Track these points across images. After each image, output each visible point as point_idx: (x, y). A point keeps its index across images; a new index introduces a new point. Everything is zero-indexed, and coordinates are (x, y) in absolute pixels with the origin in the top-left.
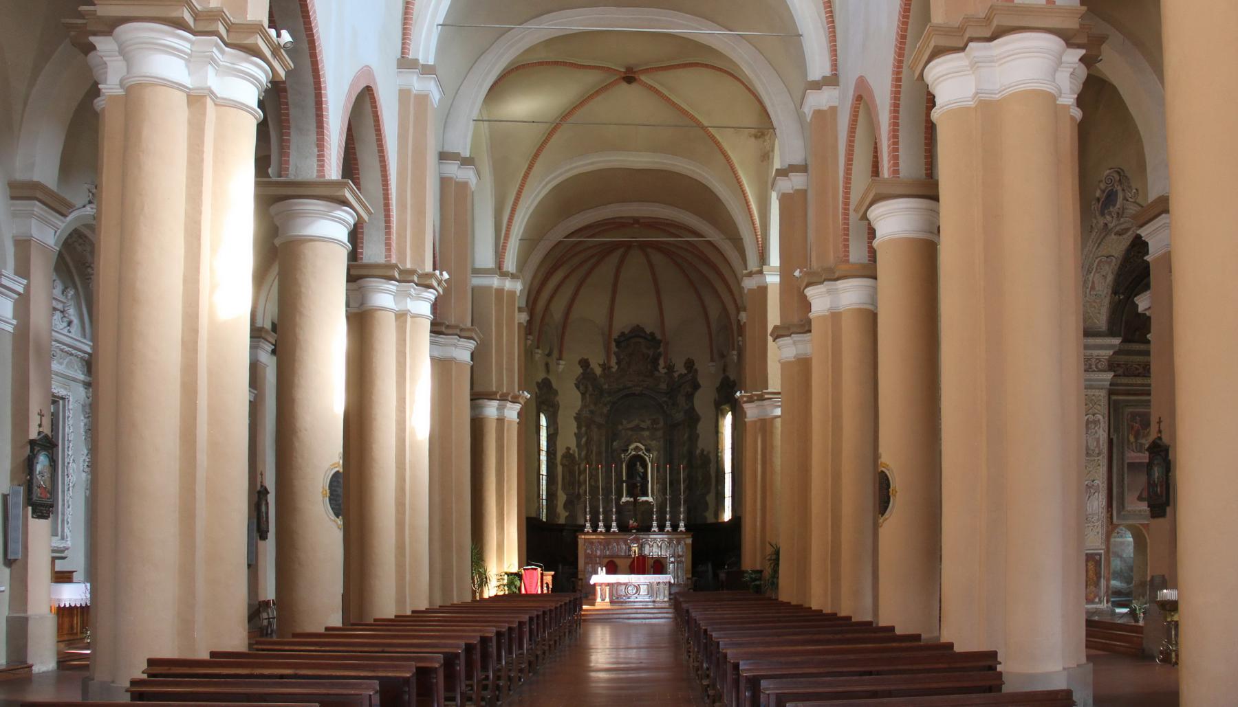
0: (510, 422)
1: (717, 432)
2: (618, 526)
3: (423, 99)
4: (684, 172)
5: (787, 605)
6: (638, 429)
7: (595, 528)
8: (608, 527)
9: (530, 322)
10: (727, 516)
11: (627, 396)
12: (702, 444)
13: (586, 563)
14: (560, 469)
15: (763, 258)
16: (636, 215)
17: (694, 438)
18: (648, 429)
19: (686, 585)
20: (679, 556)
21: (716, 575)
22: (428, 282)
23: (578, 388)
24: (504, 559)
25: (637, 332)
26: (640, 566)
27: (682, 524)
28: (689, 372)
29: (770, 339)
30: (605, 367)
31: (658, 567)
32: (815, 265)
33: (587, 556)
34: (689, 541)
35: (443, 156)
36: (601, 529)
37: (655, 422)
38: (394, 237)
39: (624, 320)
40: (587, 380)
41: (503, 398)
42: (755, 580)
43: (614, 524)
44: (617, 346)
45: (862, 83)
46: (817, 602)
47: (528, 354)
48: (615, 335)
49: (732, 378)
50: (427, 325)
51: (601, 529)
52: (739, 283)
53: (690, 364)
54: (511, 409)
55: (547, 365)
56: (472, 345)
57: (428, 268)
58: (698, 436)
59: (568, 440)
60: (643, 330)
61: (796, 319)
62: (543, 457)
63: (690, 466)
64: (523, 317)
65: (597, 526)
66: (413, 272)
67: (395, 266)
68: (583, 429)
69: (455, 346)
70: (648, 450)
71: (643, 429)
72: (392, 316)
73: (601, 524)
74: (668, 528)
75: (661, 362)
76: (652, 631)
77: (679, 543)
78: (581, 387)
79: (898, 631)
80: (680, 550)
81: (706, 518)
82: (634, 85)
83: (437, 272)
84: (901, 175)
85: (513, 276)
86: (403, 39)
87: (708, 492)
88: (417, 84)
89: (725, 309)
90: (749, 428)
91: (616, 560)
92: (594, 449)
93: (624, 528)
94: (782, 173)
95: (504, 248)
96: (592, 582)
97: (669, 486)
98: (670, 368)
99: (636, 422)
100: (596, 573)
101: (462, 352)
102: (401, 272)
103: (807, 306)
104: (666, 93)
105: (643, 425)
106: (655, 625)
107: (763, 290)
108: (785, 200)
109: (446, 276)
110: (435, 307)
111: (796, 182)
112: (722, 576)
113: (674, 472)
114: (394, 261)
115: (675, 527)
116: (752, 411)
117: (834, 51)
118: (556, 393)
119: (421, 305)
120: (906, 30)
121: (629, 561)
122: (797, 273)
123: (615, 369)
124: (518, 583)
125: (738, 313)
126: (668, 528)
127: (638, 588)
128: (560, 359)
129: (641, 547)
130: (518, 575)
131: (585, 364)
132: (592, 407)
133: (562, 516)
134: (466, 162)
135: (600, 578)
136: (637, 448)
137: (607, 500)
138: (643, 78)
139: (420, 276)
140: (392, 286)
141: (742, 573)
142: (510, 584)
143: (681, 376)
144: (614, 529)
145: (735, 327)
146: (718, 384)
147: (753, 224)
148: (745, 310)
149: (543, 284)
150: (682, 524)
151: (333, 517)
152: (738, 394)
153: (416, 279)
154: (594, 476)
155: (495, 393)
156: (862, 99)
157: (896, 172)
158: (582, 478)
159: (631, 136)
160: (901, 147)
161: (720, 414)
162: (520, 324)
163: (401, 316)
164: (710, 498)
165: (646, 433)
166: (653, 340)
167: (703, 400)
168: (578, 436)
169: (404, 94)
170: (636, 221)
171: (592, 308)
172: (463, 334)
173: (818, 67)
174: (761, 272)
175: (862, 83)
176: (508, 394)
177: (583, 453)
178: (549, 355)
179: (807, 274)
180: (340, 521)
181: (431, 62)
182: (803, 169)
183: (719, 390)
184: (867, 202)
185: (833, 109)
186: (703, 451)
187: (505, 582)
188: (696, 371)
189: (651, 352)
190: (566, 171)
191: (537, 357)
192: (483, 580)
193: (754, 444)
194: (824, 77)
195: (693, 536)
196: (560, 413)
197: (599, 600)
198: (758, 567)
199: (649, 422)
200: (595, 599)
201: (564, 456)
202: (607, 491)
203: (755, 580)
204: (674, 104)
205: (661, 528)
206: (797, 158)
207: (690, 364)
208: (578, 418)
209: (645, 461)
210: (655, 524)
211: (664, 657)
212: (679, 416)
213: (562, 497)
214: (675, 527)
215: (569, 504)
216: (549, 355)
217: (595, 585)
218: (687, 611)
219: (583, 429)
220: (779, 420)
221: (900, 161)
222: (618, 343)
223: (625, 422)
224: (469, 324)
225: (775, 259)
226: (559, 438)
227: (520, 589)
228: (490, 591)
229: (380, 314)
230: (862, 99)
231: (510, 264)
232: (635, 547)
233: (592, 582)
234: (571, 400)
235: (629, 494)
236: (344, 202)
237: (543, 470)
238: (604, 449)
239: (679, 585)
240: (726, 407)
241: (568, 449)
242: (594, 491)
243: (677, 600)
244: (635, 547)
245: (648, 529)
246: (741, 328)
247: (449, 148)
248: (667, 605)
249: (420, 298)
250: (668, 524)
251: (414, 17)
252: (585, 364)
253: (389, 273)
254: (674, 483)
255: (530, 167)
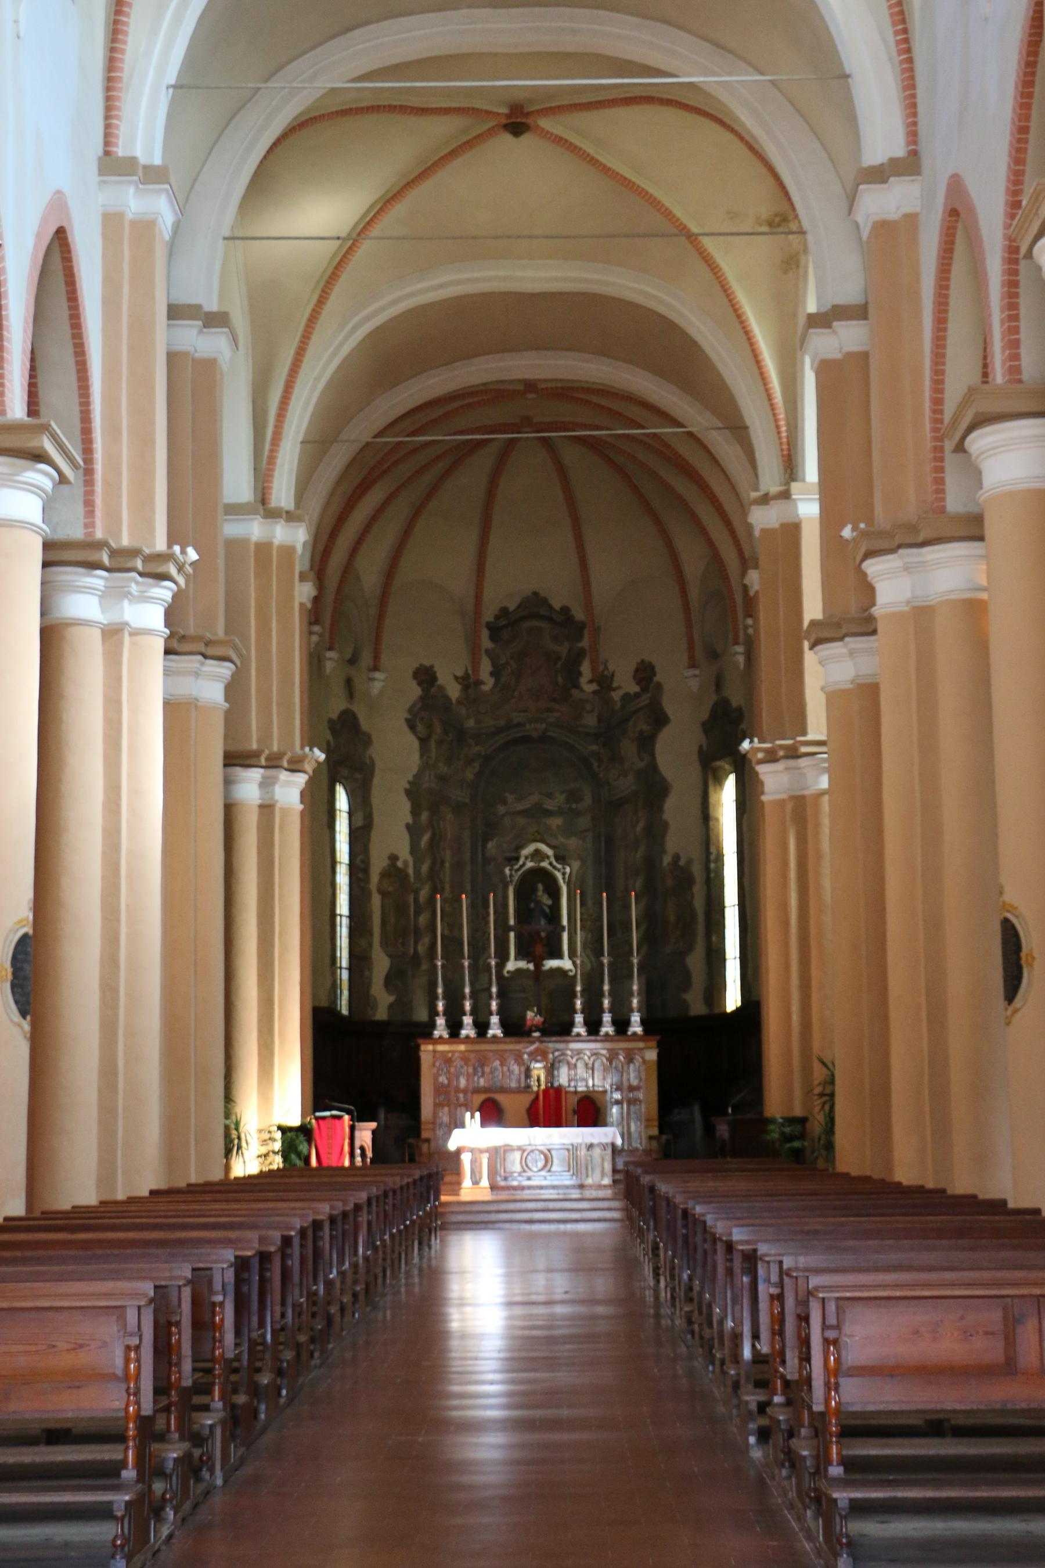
0: (285, 811)
1: (706, 817)
2: (503, 1024)
3: (145, 227)
4: (627, 295)
5: (846, 1176)
6: (538, 812)
7: (454, 1028)
8: (482, 1027)
9: (316, 600)
10: (733, 1000)
11: (517, 741)
12: (677, 843)
13: (437, 1106)
14: (376, 901)
15: (791, 468)
16: (528, 375)
17: (656, 832)
18: (560, 812)
19: (647, 1152)
20: (632, 1089)
21: (709, 1130)
22: (161, 569)
23: (412, 727)
24: (274, 1098)
25: (535, 606)
26: (549, 1109)
27: (636, 1018)
28: (644, 690)
29: (806, 644)
30: (469, 682)
31: (589, 1111)
32: (882, 517)
33: (440, 1090)
34: (652, 1055)
35: (175, 312)
36: (468, 1030)
37: (573, 796)
38: (99, 488)
39: (504, 588)
40: (430, 711)
41: (273, 763)
42: (789, 1138)
43: (495, 1020)
44: (493, 638)
45: (956, 186)
46: (905, 1174)
47: (314, 662)
48: (488, 616)
49: (735, 701)
50: (159, 645)
51: (468, 1030)
52: (744, 513)
53: (645, 673)
54: (288, 784)
55: (349, 682)
56: (225, 670)
57: (160, 544)
58: (665, 826)
59: (393, 840)
60: (545, 602)
61: (853, 608)
62: (342, 878)
63: (650, 891)
64: (304, 592)
65: (460, 1025)
66: (133, 553)
67: (99, 545)
68: (424, 816)
69: (197, 674)
70: (560, 858)
71: (549, 813)
72: (97, 634)
73: (467, 1020)
74: (607, 1028)
75: (586, 668)
76: (579, 1246)
77: (630, 1060)
78: (420, 728)
79: (1011, 1205)
80: (633, 1077)
81: (685, 1005)
82: (526, 138)
83: (177, 549)
84: (1025, 376)
85: (290, 517)
86: (107, 117)
87: (690, 948)
88: (135, 201)
89: (716, 557)
90: (768, 810)
91: (500, 1098)
92: (448, 856)
93: (514, 1029)
94: (822, 320)
95: (272, 460)
96: (452, 1145)
97: (604, 937)
98: (604, 682)
99: (535, 798)
100: (462, 1125)
101: (209, 684)
102: (114, 553)
103: (869, 591)
104: (591, 151)
105: (550, 805)
106: (586, 1234)
107: (792, 530)
108: (825, 370)
109: (192, 555)
110: (171, 616)
111: (847, 338)
112: (723, 1130)
113: (620, 906)
114: (99, 535)
115: (621, 1025)
116: (774, 781)
117: (911, 107)
118: (367, 740)
119: (148, 612)
120: (1028, 118)
121: (526, 1100)
122: (847, 532)
123: (488, 684)
124: (303, 1147)
125: (744, 574)
126: (607, 1028)
127: (548, 1159)
128: (376, 668)
129: (551, 1070)
130: (304, 1130)
131: (425, 676)
132: (444, 769)
133: (382, 1003)
134: (215, 320)
135: (471, 1137)
136: (537, 855)
137: (479, 969)
138: (544, 123)
139: (148, 559)
140: (98, 580)
141: (765, 1122)
142: (288, 1150)
143: (627, 698)
144: (495, 1030)
145: (739, 598)
146: (705, 716)
147: (770, 398)
148: (756, 567)
149: (341, 519)
150: (636, 1018)
151: (16, 1016)
152: (746, 745)
153: (139, 564)
154: (452, 919)
155: (256, 755)
156: (957, 215)
157: (1014, 371)
158: (423, 919)
159: (518, 235)
160: (1023, 324)
161: (711, 778)
162: (302, 605)
163: (113, 633)
164: (695, 961)
165: (556, 822)
166: (567, 624)
167: (675, 750)
168: (413, 831)
169: (112, 221)
170: (530, 386)
171: (443, 560)
172: (211, 651)
173: (882, 138)
174: (786, 495)
175: (956, 186)
176: (279, 756)
177: (425, 868)
178: (352, 661)
179: (863, 534)
180: (26, 1025)
181: (157, 161)
182: (859, 312)
183: (707, 727)
184: (964, 425)
185: (911, 221)
186: (676, 858)
187: (277, 1146)
188: (659, 686)
189: (563, 650)
190: (394, 302)
191: (329, 666)
192: (231, 1145)
193: (779, 847)
194: (893, 161)
195: (660, 1045)
196: (376, 781)
197: (467, 1183)
198: (798, 1112)
199: (561, 798)
200: (459, 1183)
201: (384, 875)
202: (478, 949)
203: (789, 1138)
204: (605, 170)
205: (593, 1027)
206: (850, 293)
207: (645, 673)
208: (413, 793)
209: (554, 880)
210: (579, 1018)
211: (603, 1285)
212: (625, 784)
213: (381, 963)
214: (621, 1025)
215: (395, 979)
216: (352, 661)
217: (458, 1152)
218: (652, 1189)
219: (424, 816)
220: (826, 798)
221: (1023, 351)
222: (494, 630)
223: (510, 798)
224: (221, 633)
225: (811, 471)
226: (374, 835)
227: (307, 1160)
228: (246, 1165)
229: (73, 632)
230: (957, 215)
231: (283, 494)
232: (538, 1069)
233: (452, 1145)
234: (397, 753)
235: (520, 955)
236: (39, 457)
237: (343, 905)
238: (467, 856)
239: (633, 1151)
240: (725, 764)
241: (393, 858)
242: (452, 944)
243: (632, 1185)
244: (538, 1069)
245: (562, 1029)
246: (750, 604)
247: (185, 298)
248: (609, 1193)
249: (144, 599)
250: (607, 1018)
251: (125, 75)
252: (425, 676)
253: (93, 556)
254: (619, 927)
255: (321, 302)
